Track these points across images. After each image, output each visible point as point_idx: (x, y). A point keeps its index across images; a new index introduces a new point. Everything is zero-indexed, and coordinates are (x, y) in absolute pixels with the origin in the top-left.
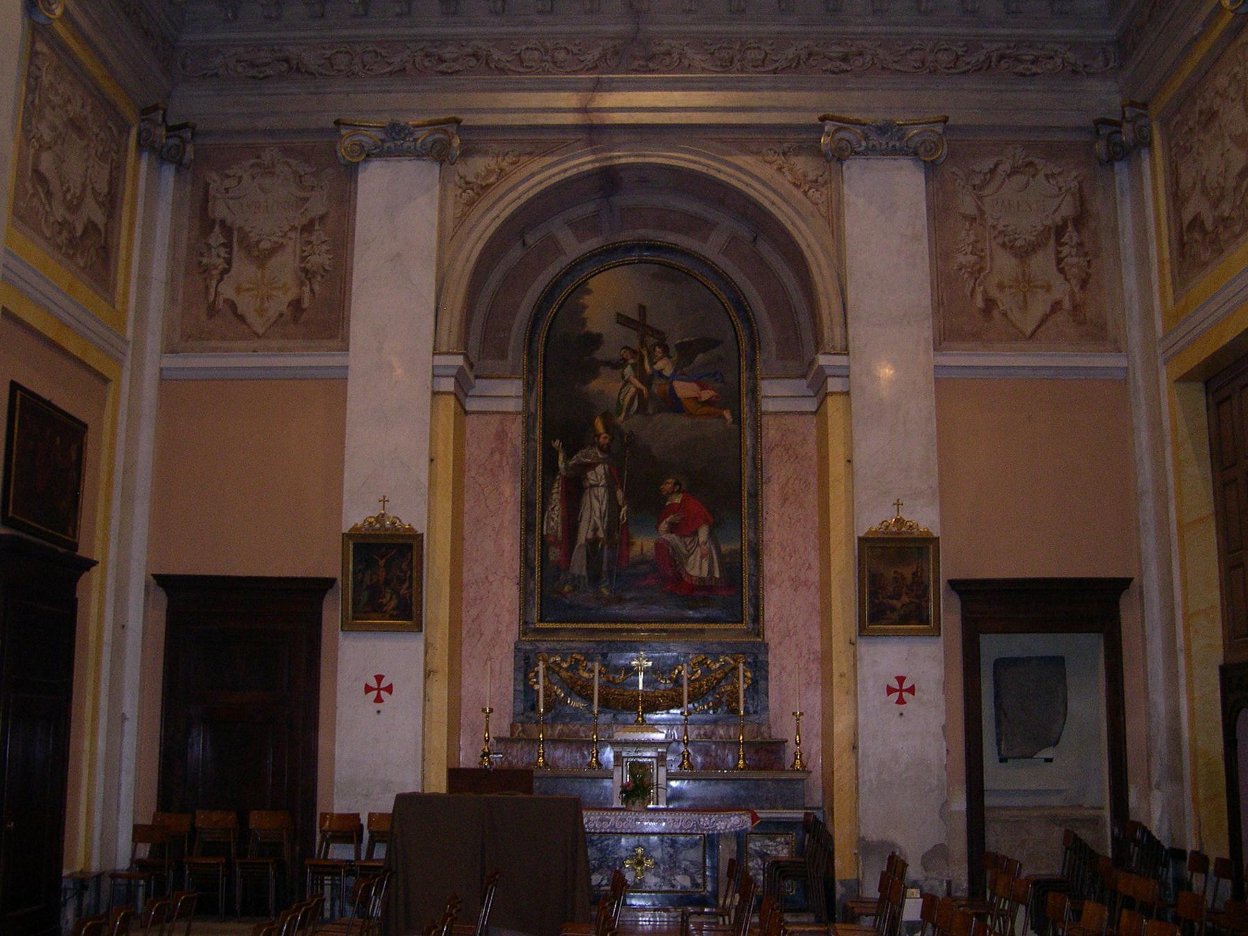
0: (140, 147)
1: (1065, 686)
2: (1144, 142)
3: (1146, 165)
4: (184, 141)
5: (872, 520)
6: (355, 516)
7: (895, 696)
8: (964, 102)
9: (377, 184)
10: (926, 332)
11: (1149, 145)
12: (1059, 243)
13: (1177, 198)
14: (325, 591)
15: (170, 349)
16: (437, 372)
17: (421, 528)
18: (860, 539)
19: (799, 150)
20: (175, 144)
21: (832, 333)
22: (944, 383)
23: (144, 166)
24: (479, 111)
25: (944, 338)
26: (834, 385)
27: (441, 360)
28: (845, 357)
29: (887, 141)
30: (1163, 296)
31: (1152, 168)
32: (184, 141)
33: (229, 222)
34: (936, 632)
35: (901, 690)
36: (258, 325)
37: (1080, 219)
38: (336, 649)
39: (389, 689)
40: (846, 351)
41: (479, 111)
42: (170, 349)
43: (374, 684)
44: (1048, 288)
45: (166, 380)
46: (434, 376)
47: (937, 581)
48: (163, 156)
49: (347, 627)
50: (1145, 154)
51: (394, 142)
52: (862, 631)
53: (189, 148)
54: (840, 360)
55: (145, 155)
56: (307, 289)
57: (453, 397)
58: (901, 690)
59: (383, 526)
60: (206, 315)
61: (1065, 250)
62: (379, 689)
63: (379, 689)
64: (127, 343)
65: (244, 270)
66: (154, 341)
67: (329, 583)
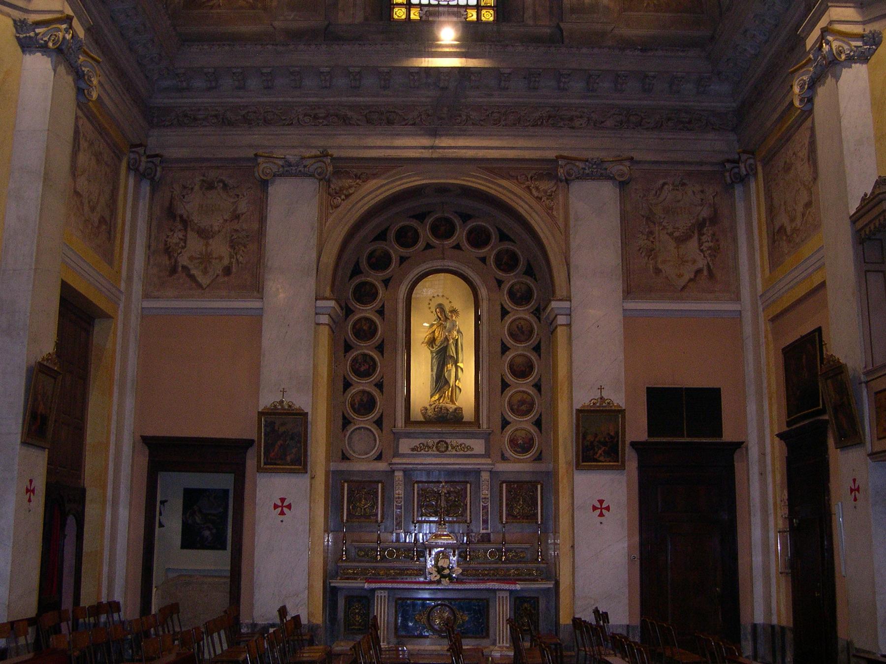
0: (129, 168)
1: (872, 94)
2: (752, 171)
3: (753, 185)
4: (156, 166)
5: (584, 398)
6: (267, 400)
7: (598, 512)
8: (644, 146)
9: (281, 193)
10: (618, 285)
11: (755, 175)
12: (701, 234)
13: (771, 211)
14: (247, 448)
15: (146, 296)
16: (318, 311)
17: (308, 409)
18: (577, 410)
19: (540, 176)
20: (152, 171)
21: (560, 292)
22: (629, 318)
23: (131, 181)
24: (340, 147)
25: (628, 293)
26: (561, 320)
27: (320, 303)
28: (569, 303)
29: (596, 171)
30: (763, 271)
31: (756, 187)
32: (156, 166)
33: (185, 216)
34: (622, 467)
35: (601, 509)
36: (204, 280)
37: (714, 219)
38: (255, 485)
39: (289, 507)
40: (569, 299)
41: (340, 147)
42: (146, 296)
43: (279, 503)
44: (694, 261)
45: (146, 315)
46: (316, 314)
47: (624, 442)
48: (141, 176)
49: (259, 469)
50: (752, 179)
51: (290, 170)
52: (578, 467)
53: (159, 169)
54: (566, 304)
55: (132, 173)
56: (234, 260)
57: (327, 327)
58: (601, 508)
59: (282, 406)
60: (170, 269)
61: (704, 238)
62: (283, 506)
63: (282, 507)
64: (121, 292)
65: (195, 245)
66: (137, 288)
67: (249, 443)
